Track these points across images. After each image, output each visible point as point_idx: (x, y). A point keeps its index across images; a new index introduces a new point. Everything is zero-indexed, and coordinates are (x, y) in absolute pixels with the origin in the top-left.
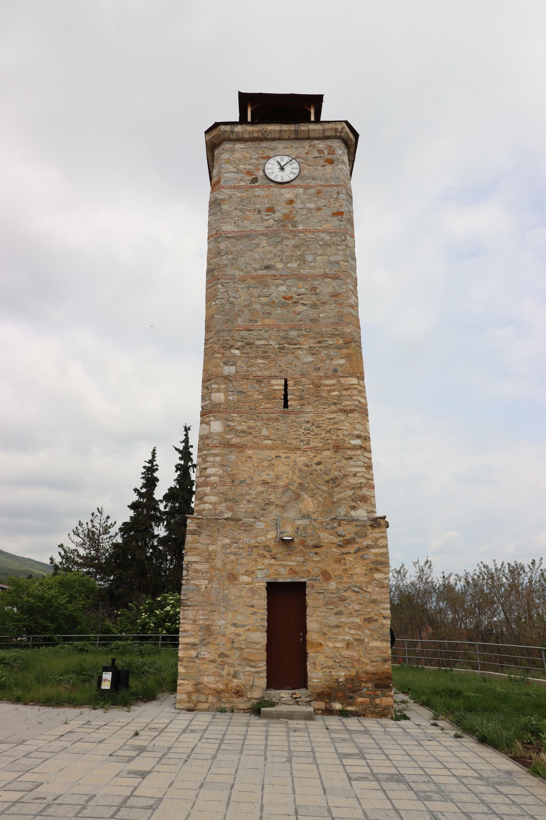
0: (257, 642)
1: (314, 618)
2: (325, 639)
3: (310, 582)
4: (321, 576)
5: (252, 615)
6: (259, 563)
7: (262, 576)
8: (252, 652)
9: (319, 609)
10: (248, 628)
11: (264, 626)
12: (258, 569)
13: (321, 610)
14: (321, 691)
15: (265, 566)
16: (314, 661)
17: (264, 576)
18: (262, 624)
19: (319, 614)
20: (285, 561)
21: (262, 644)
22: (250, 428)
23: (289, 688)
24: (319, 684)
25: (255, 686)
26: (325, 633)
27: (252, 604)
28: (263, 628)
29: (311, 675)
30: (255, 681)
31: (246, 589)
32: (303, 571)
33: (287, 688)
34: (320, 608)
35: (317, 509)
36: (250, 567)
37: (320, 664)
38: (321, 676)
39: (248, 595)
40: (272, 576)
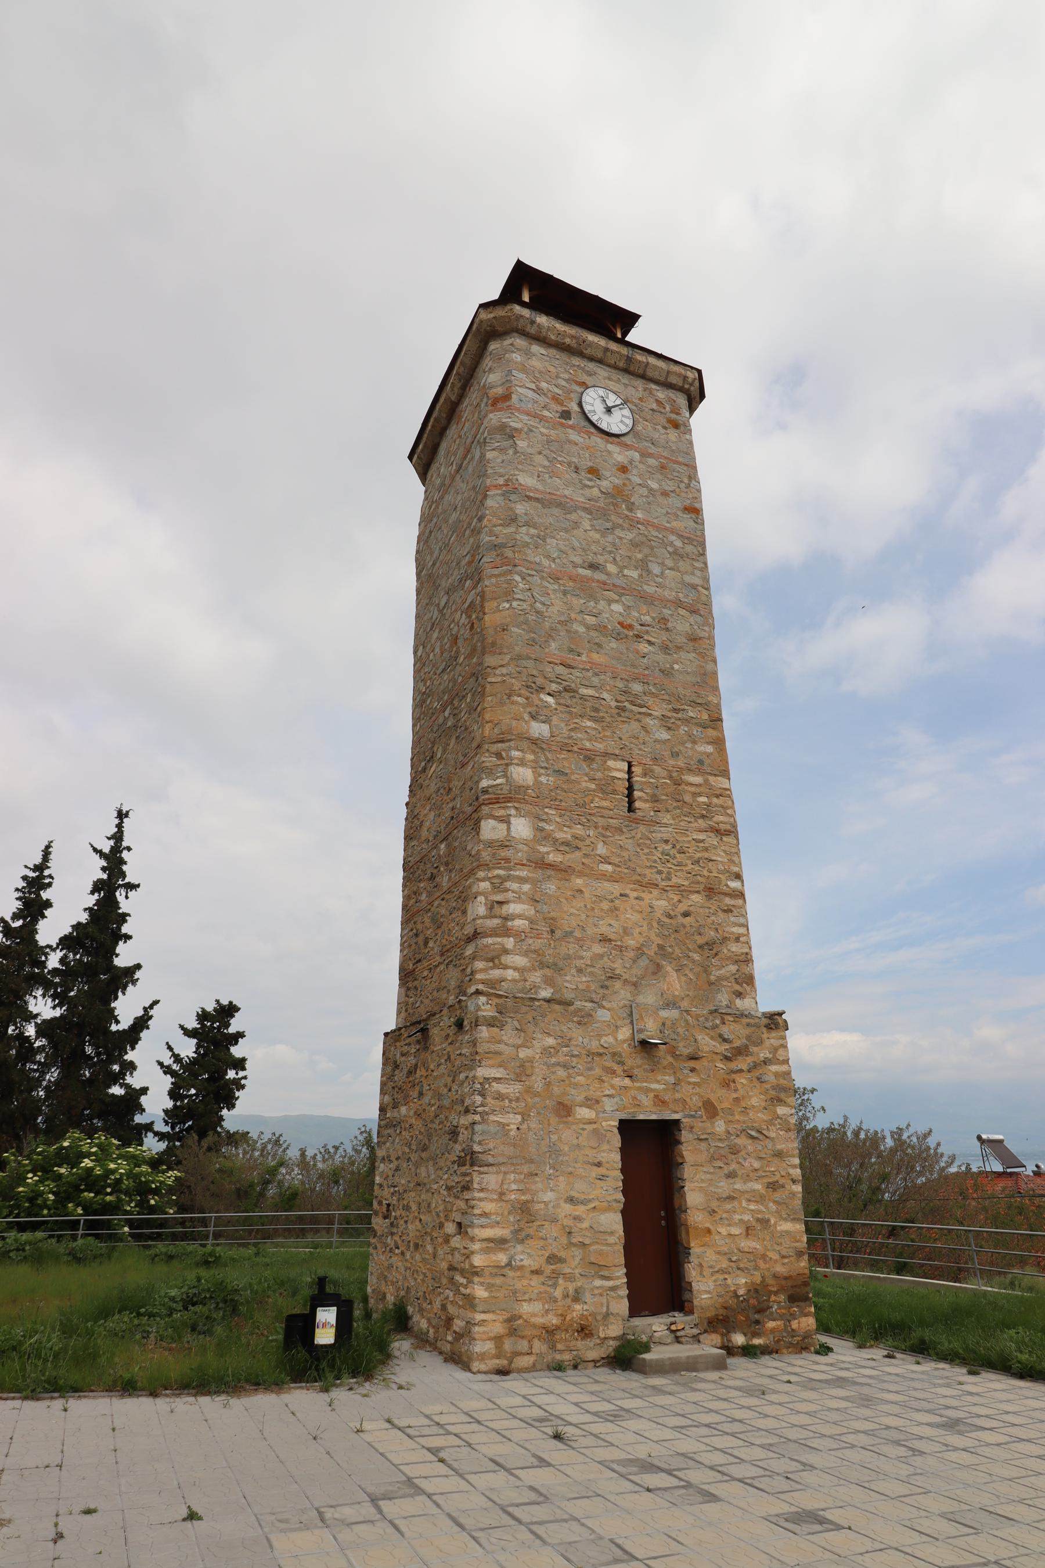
2: (715, 1221)
8: (601, 1250)
10: (593, 1205)
13: (705, 1169)
20: (646, 1082)
23: (647, 1313)
29: (697, 1288)
30: (611, 1304)
34: (703, 1166)
38: (712, 1287)
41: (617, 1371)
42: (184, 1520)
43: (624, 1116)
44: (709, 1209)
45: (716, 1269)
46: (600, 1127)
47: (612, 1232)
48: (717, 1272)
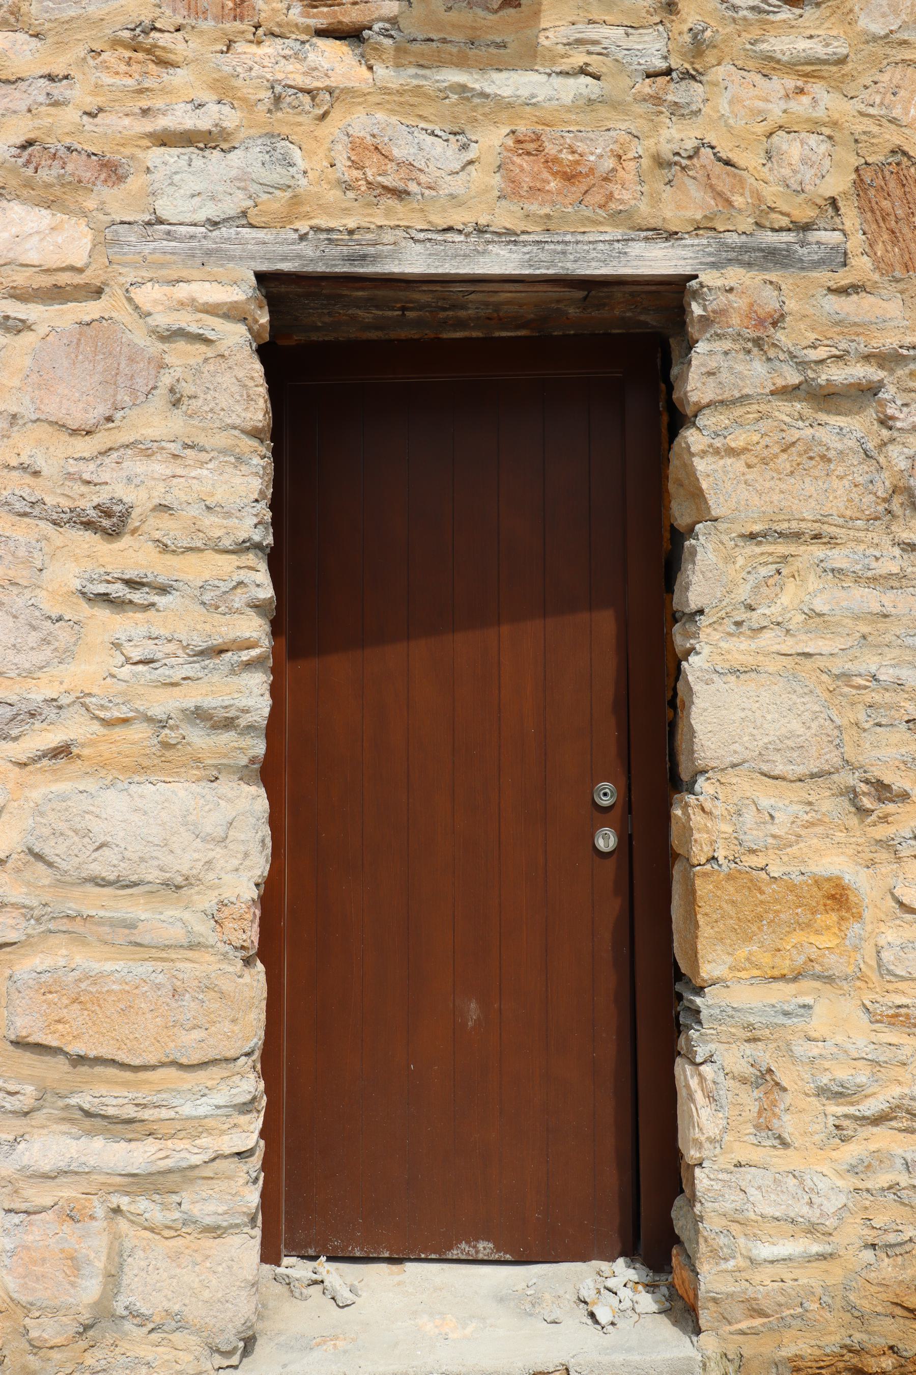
0: (153, 875)
1: (768, 640)
2: (885, 844)
3: (735, 275)
4: (850, 217)
5: (103, 613)
6: (179, 77)
7: (210, 211)
8: (96, 979)
9: (818, 551)
10: (53, 738)
11: (228, 724)
12: (164, 139)
13: (838, 558)
14: (833, 1341)
15: (250, 105)
16: (764, 1055)
17: (230, 206)
18: (208, 702)
19: (819, 605)
20: (461, 62)
21: (208, 901)
22: (216, 224)
23: (484, 1248)
24: (810, 1277)
25: (133, 1314)
26: (882, 789)
27: (102, 497)
28: (227, 738)
29: (731, 1201)
30: (133, 1266)
31: (27, 338)
32: (660, 163)
33: (463, 1249)
34: (832, 542)
35: (210, 234)
36: (71, 116)
37: (822, 1092)
38: (832, 1204)
39: (53, 409)
40: (325, 209)
41: (638, 1265)
42: (12, 1042)
43: (264, 267)
44: (850, 779)
45: (870, 1107)
46: (124, 315)
47: (173, 887)
48: (877, 1120)
